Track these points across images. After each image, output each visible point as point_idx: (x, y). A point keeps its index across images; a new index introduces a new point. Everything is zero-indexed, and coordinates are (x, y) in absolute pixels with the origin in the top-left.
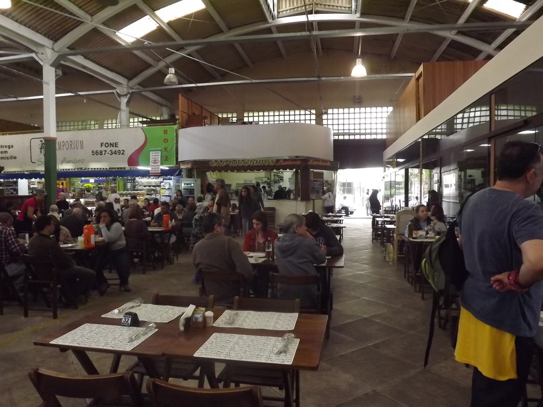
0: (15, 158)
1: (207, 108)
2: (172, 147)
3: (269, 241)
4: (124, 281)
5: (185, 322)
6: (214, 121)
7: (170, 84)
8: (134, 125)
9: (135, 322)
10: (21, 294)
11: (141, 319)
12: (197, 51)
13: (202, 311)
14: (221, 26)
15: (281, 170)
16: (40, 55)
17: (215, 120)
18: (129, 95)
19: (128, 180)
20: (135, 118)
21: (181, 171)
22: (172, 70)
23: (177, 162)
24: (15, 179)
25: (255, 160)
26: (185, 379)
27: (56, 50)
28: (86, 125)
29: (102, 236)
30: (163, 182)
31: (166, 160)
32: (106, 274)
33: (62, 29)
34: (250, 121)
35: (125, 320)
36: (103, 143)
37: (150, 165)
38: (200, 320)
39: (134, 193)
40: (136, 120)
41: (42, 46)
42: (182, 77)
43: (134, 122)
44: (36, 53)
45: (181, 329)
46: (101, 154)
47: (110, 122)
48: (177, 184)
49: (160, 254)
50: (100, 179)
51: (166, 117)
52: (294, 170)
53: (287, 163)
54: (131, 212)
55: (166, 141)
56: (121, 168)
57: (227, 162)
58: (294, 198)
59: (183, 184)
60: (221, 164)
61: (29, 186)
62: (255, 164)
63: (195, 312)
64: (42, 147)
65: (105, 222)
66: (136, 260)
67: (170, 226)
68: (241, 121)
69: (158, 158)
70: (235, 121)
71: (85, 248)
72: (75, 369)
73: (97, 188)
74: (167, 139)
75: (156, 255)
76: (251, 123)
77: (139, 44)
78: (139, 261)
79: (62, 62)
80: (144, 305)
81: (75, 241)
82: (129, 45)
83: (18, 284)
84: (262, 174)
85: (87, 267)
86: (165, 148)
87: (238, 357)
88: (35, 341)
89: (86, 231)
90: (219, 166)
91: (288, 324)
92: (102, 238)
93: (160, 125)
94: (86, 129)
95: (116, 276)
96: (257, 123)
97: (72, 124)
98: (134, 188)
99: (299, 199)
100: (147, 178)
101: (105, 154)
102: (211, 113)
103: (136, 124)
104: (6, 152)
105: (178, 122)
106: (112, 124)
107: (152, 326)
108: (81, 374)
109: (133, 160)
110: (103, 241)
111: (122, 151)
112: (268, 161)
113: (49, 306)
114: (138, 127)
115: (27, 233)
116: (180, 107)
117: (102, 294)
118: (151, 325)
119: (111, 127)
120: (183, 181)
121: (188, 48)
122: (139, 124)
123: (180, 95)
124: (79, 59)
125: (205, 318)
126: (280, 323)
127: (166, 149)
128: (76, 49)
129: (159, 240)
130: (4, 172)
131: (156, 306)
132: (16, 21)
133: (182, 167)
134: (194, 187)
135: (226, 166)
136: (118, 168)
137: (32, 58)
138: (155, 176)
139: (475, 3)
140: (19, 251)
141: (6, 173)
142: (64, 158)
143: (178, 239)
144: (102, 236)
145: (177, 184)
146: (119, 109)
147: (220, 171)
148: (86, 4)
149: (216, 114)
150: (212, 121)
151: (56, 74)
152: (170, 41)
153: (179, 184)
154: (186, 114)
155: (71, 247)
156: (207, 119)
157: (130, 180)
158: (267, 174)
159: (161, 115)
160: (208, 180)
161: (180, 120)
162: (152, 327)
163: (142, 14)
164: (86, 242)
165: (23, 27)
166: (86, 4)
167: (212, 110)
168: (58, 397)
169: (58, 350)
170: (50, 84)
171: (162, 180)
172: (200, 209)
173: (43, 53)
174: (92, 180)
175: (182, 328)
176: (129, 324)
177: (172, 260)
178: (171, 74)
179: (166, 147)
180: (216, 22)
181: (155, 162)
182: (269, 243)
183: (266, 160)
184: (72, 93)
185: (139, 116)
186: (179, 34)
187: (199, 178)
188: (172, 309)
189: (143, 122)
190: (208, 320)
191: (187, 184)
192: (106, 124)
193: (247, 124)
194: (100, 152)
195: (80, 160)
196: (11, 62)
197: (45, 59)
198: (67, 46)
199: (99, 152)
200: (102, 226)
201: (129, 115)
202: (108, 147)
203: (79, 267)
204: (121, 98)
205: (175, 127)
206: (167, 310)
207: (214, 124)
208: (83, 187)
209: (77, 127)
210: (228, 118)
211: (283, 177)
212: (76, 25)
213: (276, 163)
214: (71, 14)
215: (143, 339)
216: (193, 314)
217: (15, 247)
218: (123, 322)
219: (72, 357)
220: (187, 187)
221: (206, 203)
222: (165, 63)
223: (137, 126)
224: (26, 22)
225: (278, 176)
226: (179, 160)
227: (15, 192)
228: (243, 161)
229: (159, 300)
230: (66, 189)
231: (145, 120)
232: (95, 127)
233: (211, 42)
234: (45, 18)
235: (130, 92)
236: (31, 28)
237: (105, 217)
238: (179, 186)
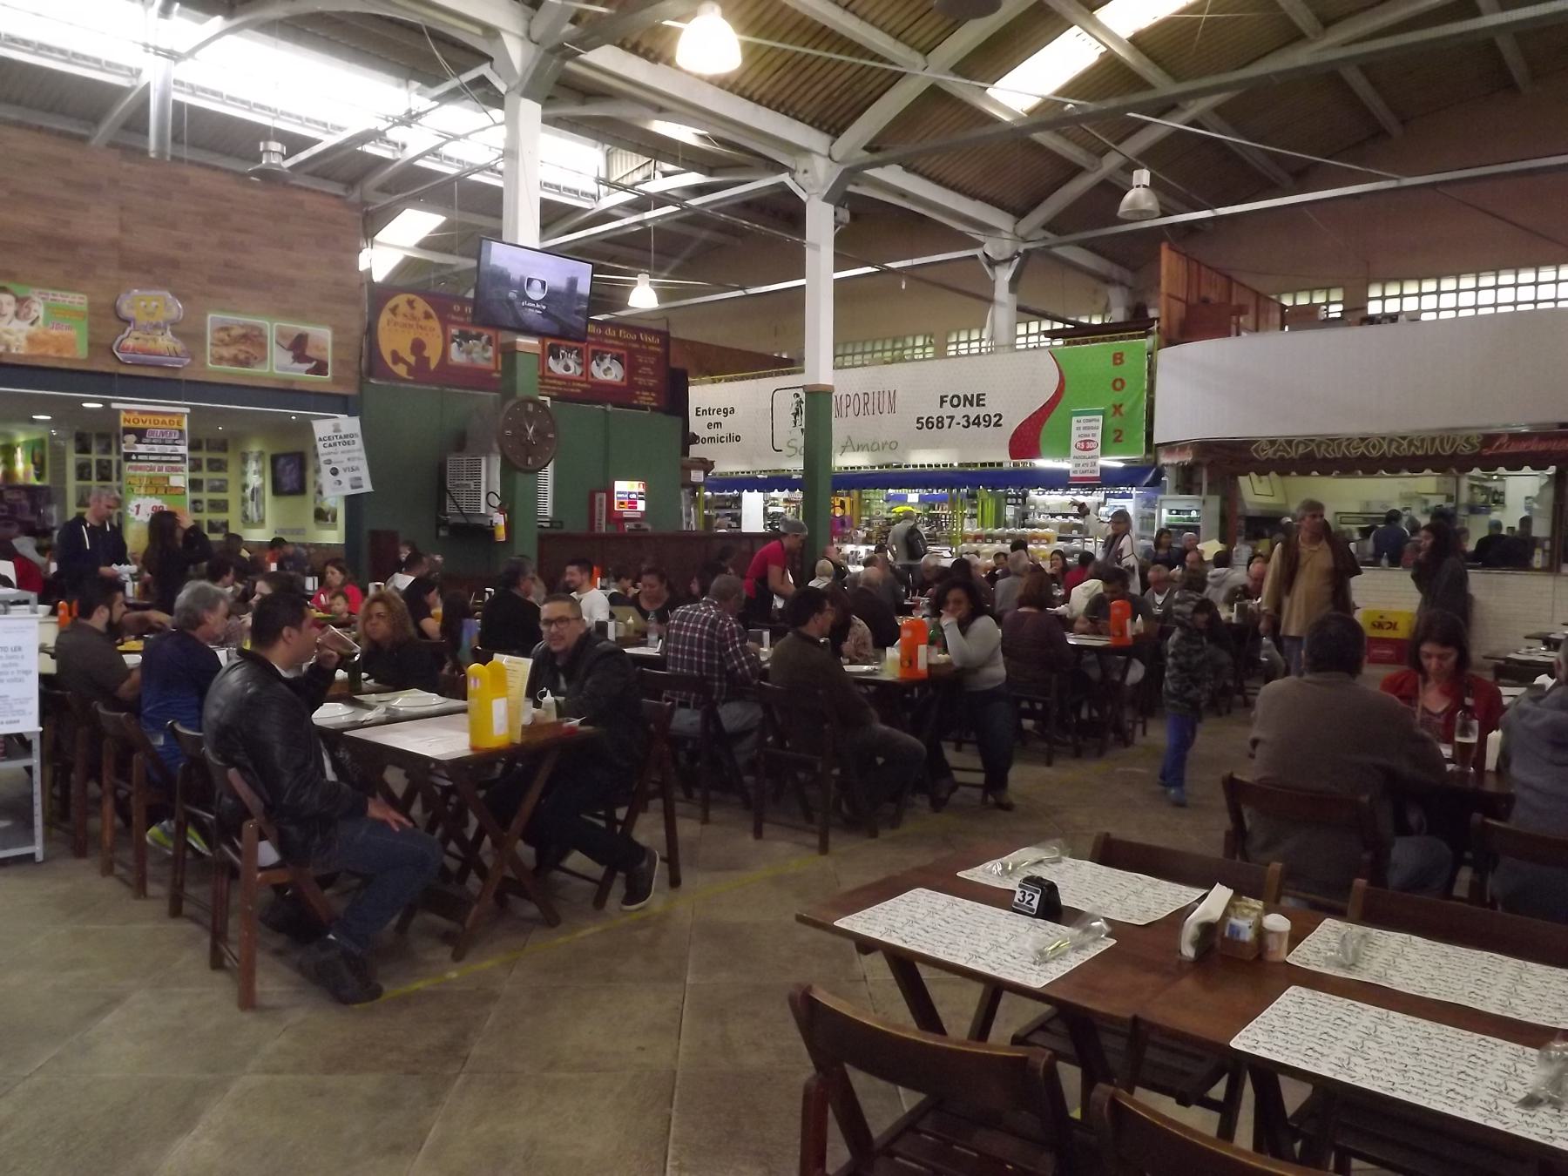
0: (738, 439)
1: (1245, 280)
2: (1139, 398)
3: (1467, 709)
4: (996, 780)
5: (1199, 934)
6: (1267, 321)
7: (1138, 217)
8: (1027, 343)
9: (1051, 908)
10: (748, 779)
11: (1066, 900)
12: (1217, 110)
13: (1254, 909)
14: (1296, 19)
15: (1502, 470)
16: (799, 176)
17: (1271, 316)
18: (1016, 261)
19: (1007, 497)
20: (1031, 324)
21: (1160, 473)
22: (1143, 176)
23: (1150, 446)
24: (736, 492)
25: (1404, 438)
26: (1184, 1101)
27: (836, 158)
28: (903, 349)
29: (946, 651)
30: (1104, 504)
31: (1117, 440)
32: (950, 754)
33: (853, 102)
34: (1388, 310)
35: (1024, 896)
36: (946, 396)
37: (1072, 455)
38: (1248, 935)
39: (1024, 535)
40: (1034, 327)
41: (805, 151)
42: (1169, 194)
43: (1028, 335)
44: (792, 172)
45: (1184, 952)
46: (940, 425)
47: (963, 337)
48: (1148, 511)
49: (1095, 714)
50: (935, 492)
51: (1118, 315)
52: (1552, 470)
53: (1522, 447)
54: (1025, 590)
55: (1118, 385)
56: (991, 464)
58: (1547, 564)
59: (1165, 512)
60: (1288, 453)
61: (765, 509)
62: (1405, 450)
63: (1231, 910)
64: (797, 409)
65: (957, 614)
66: (1028, 723)
67: (1130, 633)
68: (1360, 315)
69: (1094, 435)
70: (1339, 315)
71: (902, 678)
72: (870, 994)
73: (926, 519)
74: (1122, 380)
75: (1084, 714)
76: (1393, 318)
77: (1049, 114)
78: (1035, 727)
79: (851, 188)
80: (1072, 861)
81: (879, 659)
82: (1020, 119)
83: (744, 751)
84: (1427, 483)
85: (905, 731)
86: (1115, 406)
87: (1535, 1129)
88: (799, 913)
89: (906, 634)
90: (1282, 458)
91: (1560, 1008)
92: (946, 656)
93: (1104, 340)
94: (902, 360)
95: (978, 763)
96: (1414, 317)
97: (868, 348)
98: (1023, 519)
99: (1384, 562)
100: (1060, 491)
101: (949, 427)
102: (1257, 293)
103: (1035, 339)
104: (718, 424)
105: (1155, 327)
106: (969, 341)
107: (1101, 927)
108: (895, 1016)
109: (1026, 441)
110: (949, 664)
111: (995, 416)
112: (1454, 441)
113: (809, 818)
114: (1040, 348)
115: (765, 628)
116: (1164, 283)
117: (938, 805)
118: (1098, 923)
119: (965, 352)
120: (1164, 504)
121: (1192, 103)
122: (1043, 338)
123: (1164, 247)
124: (893, 175)
125: (1261, 933)
126: (1405, 967)
127: (1117, 408)
128: (886, 149)
129: (1095, 673)
130: (714, 474)
131: (1105, 869)
132: (750, 98)
133: (1164, 460)
134: (1198, 519)
136: (983, 464)
137: (783, 185)
138: (1083, 486)
140: (749, 674)
141: (717, 476)
142: (849, 438)
143: (1149, 675)
144: (946, 651)
145: (1148, 511)
146: (990, 301)
147: (1283, 472)
148: (915, 22)
149: (1274, 297)
150: (1262, 321)
151: (835, 221)
152: (1138, 90)
153: (1152, 511)
154: (1179, 303)
155: (867, 673)
156: (1247, 313)
157: (1012, 497)
158: (1445, 483)
159: (1106, 310)
160: (1242, 500)
161: (1163, 324)
162: (1100, 930)
163: (1061, 25)
164: (907, 664)
165: (763, 111)
166: (915, 22)
167: (1260, 284)
168: (847, 1066)
169: (852, 944)
170: (823, 248)
171: (1102, 499)
172: (1218, 586)
173: (808, 168)
174: (913, 497)
175: (1188, 951)
176: (1032, 910)
177: (1130, 734)
178: (1138, 186)
179: (1118, 404)
180: (1281, 9)
181: (1085, 445)
182: (1468, 716)
183: (1448, 435)
184: (873, 267)
185: (1042, 316)
186: (1162, 67)
187: (1215, 494)
188: (1075, 867)
189: (1052, 334)
190: (1272, 942)
191: (1178, 512)
192: (953, 343)
193: (1379, 323)
194: (938, 422)
195: (886, 443)
196: (736, 201)
197: (811, 185)
198: (864, 144)
199: (935, 421)
200: (947, 621)
201: (1017, 316)
202: (958, 405)
203: (886, 728)
204: (997, 268)
205: (1148, 342)
206: (1139, 887)
207: (1267, 330)
208: (890, 515)
209: (880, 355)
210: (1312, 309)
211: (1502, 494)
212: (888, 83)
213: (1483, 447)
214: (875, 57)
215: (1074, 961)
216: (1226, 914)
217: (741, 665)
218: (1016, 900)
219: (877, 967)
220: (1178, 519)
221: (1238, 575)
222: (1122, 158)
223: (1037, 345)
224: (770, 96)
225: (1486, 490)
226: (1157, 440)
227: (734, 525)
228: (1363, 440)
229: (1112, 854)
230: (851, 519)
231: (1058, 326)
232: (969, 349)
233: (1267, 76)
234: (815, 79)
235: (1021, 251)
236: (782, 110)
237: (958, 602)
238: (1153, 516)
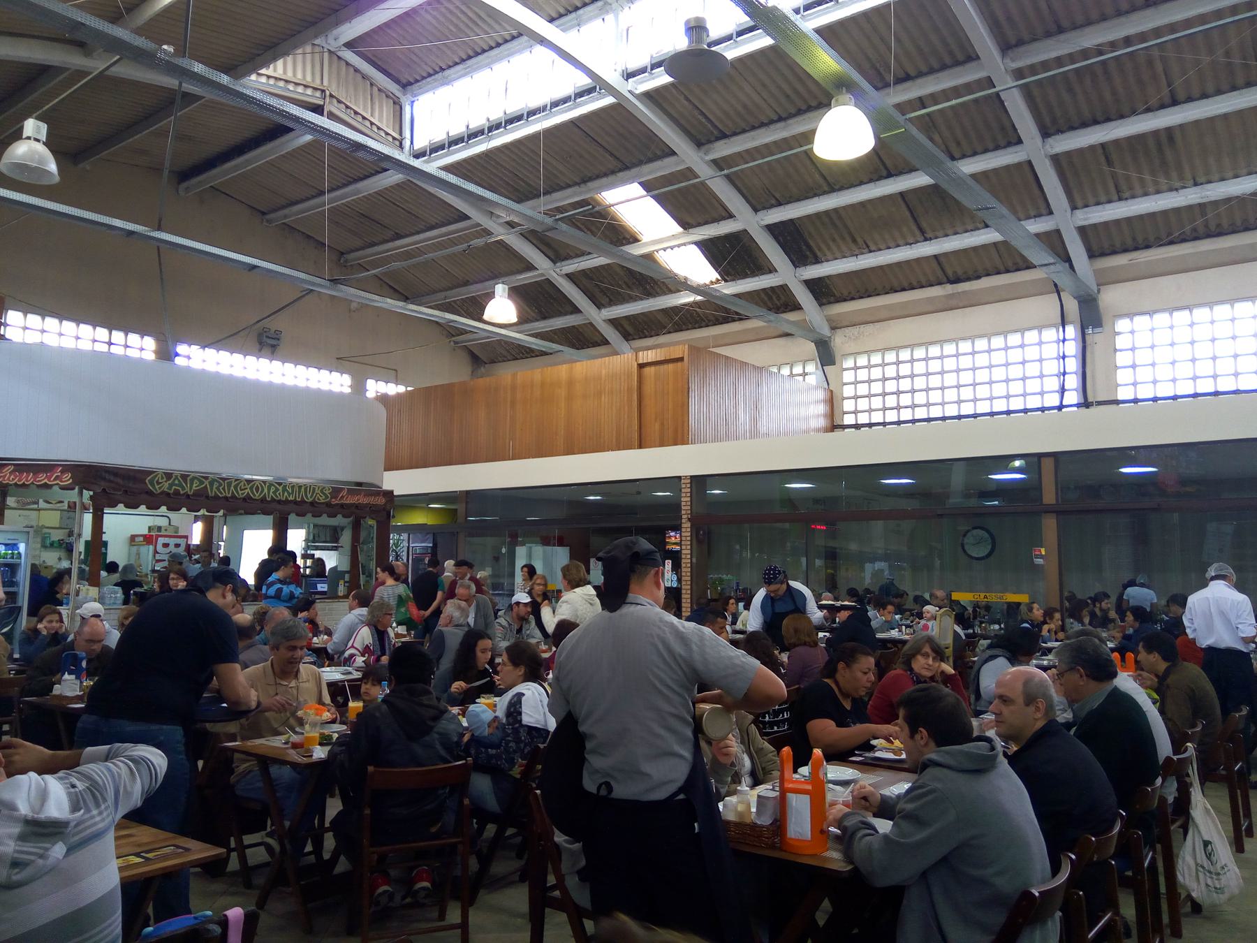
57: (202, 483)
90: (177, 493)
112: (314, 489)
135: (198, 494)
139: (1223, 4)
213: (331, 498)
